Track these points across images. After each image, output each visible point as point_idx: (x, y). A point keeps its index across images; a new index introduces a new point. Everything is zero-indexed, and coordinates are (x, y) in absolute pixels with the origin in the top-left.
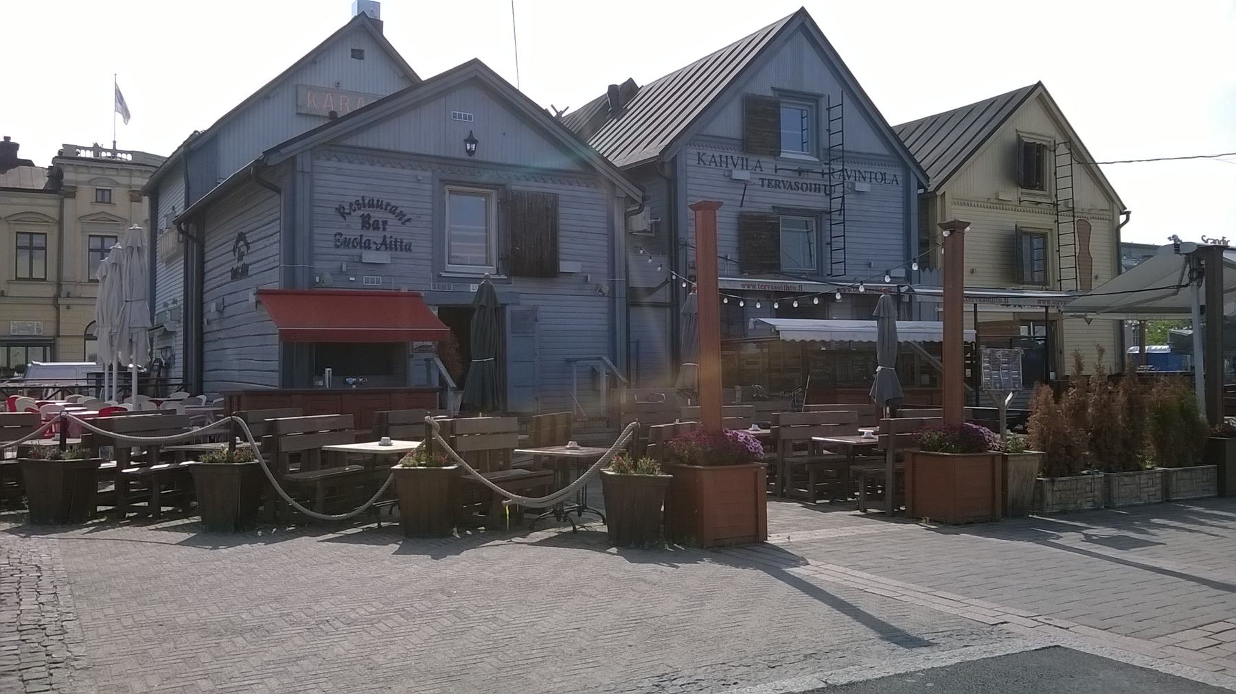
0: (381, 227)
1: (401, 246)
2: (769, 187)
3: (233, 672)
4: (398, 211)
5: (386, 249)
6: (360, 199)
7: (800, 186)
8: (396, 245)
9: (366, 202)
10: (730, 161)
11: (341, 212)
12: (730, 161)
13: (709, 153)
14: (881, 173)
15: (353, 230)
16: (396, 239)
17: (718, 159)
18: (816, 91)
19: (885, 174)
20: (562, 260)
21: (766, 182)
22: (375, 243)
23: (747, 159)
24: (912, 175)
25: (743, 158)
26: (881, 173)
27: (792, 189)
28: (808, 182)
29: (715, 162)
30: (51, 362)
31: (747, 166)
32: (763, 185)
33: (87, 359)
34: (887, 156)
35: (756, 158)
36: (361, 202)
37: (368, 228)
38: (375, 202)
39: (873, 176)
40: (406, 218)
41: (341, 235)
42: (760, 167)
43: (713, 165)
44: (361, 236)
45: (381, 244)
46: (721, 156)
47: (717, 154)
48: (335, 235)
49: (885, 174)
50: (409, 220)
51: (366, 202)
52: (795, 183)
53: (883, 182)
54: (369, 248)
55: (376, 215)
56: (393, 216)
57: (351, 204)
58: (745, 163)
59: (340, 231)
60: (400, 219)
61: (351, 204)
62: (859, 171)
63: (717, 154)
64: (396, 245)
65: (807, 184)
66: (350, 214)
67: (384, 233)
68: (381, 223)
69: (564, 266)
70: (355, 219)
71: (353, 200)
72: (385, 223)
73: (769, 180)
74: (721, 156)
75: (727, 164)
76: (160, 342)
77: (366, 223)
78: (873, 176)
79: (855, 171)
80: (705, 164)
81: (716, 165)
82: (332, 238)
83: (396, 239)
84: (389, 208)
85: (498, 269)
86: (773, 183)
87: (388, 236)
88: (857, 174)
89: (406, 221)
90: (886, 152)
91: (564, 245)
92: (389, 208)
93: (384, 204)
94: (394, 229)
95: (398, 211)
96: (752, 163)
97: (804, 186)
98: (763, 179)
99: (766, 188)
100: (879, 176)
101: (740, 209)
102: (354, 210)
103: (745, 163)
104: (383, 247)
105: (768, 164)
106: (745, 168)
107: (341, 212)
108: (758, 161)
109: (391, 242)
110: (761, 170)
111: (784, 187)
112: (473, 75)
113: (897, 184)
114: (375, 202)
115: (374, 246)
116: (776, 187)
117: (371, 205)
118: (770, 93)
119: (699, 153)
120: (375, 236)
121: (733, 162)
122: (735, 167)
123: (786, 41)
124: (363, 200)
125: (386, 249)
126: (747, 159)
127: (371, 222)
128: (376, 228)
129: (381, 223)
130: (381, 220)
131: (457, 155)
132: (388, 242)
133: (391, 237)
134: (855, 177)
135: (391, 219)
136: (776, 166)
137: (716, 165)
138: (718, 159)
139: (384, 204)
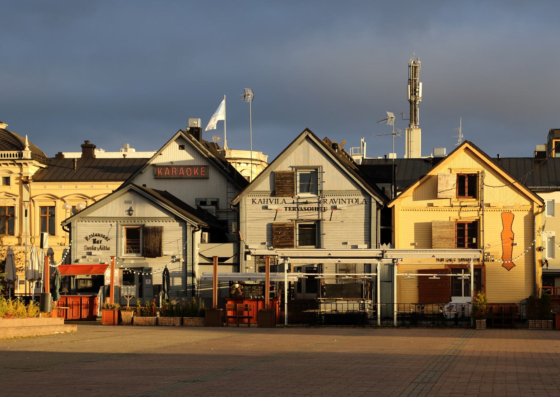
0: (99, 242)
1: (106, 248)
4: (105, 237)
5: (101, 250)
7: (307, 209)
8: (104, 248)
9: (95, 235)
10: (269, 201)
11: (86, 238)
12: (269, 201)
13: (258, 198)
14: (356, 199)
15: (90, 244)
16: (104, 246)
17: (263, 201)
19: (358, 199)
20: (165, 250)
21: (288, 209)
22: (97, 248)
23: (278, 199)
24: (373, 200)
26: (356, 199)
28: (311, 207)
29: (261, 202)
30: (339, 273)
31: (278, 202)
32: (286, 210)
33: (292, 270)
34: (356, 191)
35: (283, 198)
36: (93, 235)
37: (95, 243)
38: (98, 235)
39: (351, 201)
40: (108, 239)
41: (86, 246)
42: (285, 202)
43: (260, 203)
44: (93, 246)
46: (264, 199)
47: (262, 198)
48: (84, 246)
49: (358, 199)
50: (109, 240)
51: (95, 235)
53: (357, 203)
54: (95, 250)
55: (98, 238)
56: (104, 239)
57: (90, 236)
58: (277, 201)
59: (86, 245)
60: (106, 240)
61: (90, 236)
62: (342, 199)
64: (104, 248)
65: (311, 208)
66: (89, 239)
67: (101, 244)
68: (99, 241)
69: (165, 252)
70: (91, 241)
72: (101, 241)
73: (289, 208)
74: (264, 199)
76: (281, 261)
77: (95, 241)
78: (351, 201)
79: (339, 199)
80: (256, 203)
81: (262, 203)
82: (83, 247)
83: (104, 246)
84: (102, 236)
85: (142, 255)
87: (102, 245)
88: (341, 201)
89: (108, 240)
90: (355, 189)
92: (102, 236)
93: (101, 235)
94: (104, 243)
95: (105, 237)
96: (281, 199)
97: (309, 208)
100: (354, 201)
103: (277, 201)
104: (100, 249)
105: (289, 200)
106: (277, 203)
107: (87, 238)
108: (284, 200)
109: (103, 247)
112: (130, 188)
114: (98, 235)
115: (97, 249)
117: (96, 235)
119: (253, 199)
120: (97, 245)
121: (271, 201)
122: (271, 203)
123: (300, 144)
124: (94, 234)
125: (101, 250)
127: (96, 241)
128: (98, 243)
130: (99, 240)
131: (125, 216)
132: (102, 248)
133: (103, 246)
135: (104, 241)
137: (262, 203)
138: (263, 201)
139: (101, 235)
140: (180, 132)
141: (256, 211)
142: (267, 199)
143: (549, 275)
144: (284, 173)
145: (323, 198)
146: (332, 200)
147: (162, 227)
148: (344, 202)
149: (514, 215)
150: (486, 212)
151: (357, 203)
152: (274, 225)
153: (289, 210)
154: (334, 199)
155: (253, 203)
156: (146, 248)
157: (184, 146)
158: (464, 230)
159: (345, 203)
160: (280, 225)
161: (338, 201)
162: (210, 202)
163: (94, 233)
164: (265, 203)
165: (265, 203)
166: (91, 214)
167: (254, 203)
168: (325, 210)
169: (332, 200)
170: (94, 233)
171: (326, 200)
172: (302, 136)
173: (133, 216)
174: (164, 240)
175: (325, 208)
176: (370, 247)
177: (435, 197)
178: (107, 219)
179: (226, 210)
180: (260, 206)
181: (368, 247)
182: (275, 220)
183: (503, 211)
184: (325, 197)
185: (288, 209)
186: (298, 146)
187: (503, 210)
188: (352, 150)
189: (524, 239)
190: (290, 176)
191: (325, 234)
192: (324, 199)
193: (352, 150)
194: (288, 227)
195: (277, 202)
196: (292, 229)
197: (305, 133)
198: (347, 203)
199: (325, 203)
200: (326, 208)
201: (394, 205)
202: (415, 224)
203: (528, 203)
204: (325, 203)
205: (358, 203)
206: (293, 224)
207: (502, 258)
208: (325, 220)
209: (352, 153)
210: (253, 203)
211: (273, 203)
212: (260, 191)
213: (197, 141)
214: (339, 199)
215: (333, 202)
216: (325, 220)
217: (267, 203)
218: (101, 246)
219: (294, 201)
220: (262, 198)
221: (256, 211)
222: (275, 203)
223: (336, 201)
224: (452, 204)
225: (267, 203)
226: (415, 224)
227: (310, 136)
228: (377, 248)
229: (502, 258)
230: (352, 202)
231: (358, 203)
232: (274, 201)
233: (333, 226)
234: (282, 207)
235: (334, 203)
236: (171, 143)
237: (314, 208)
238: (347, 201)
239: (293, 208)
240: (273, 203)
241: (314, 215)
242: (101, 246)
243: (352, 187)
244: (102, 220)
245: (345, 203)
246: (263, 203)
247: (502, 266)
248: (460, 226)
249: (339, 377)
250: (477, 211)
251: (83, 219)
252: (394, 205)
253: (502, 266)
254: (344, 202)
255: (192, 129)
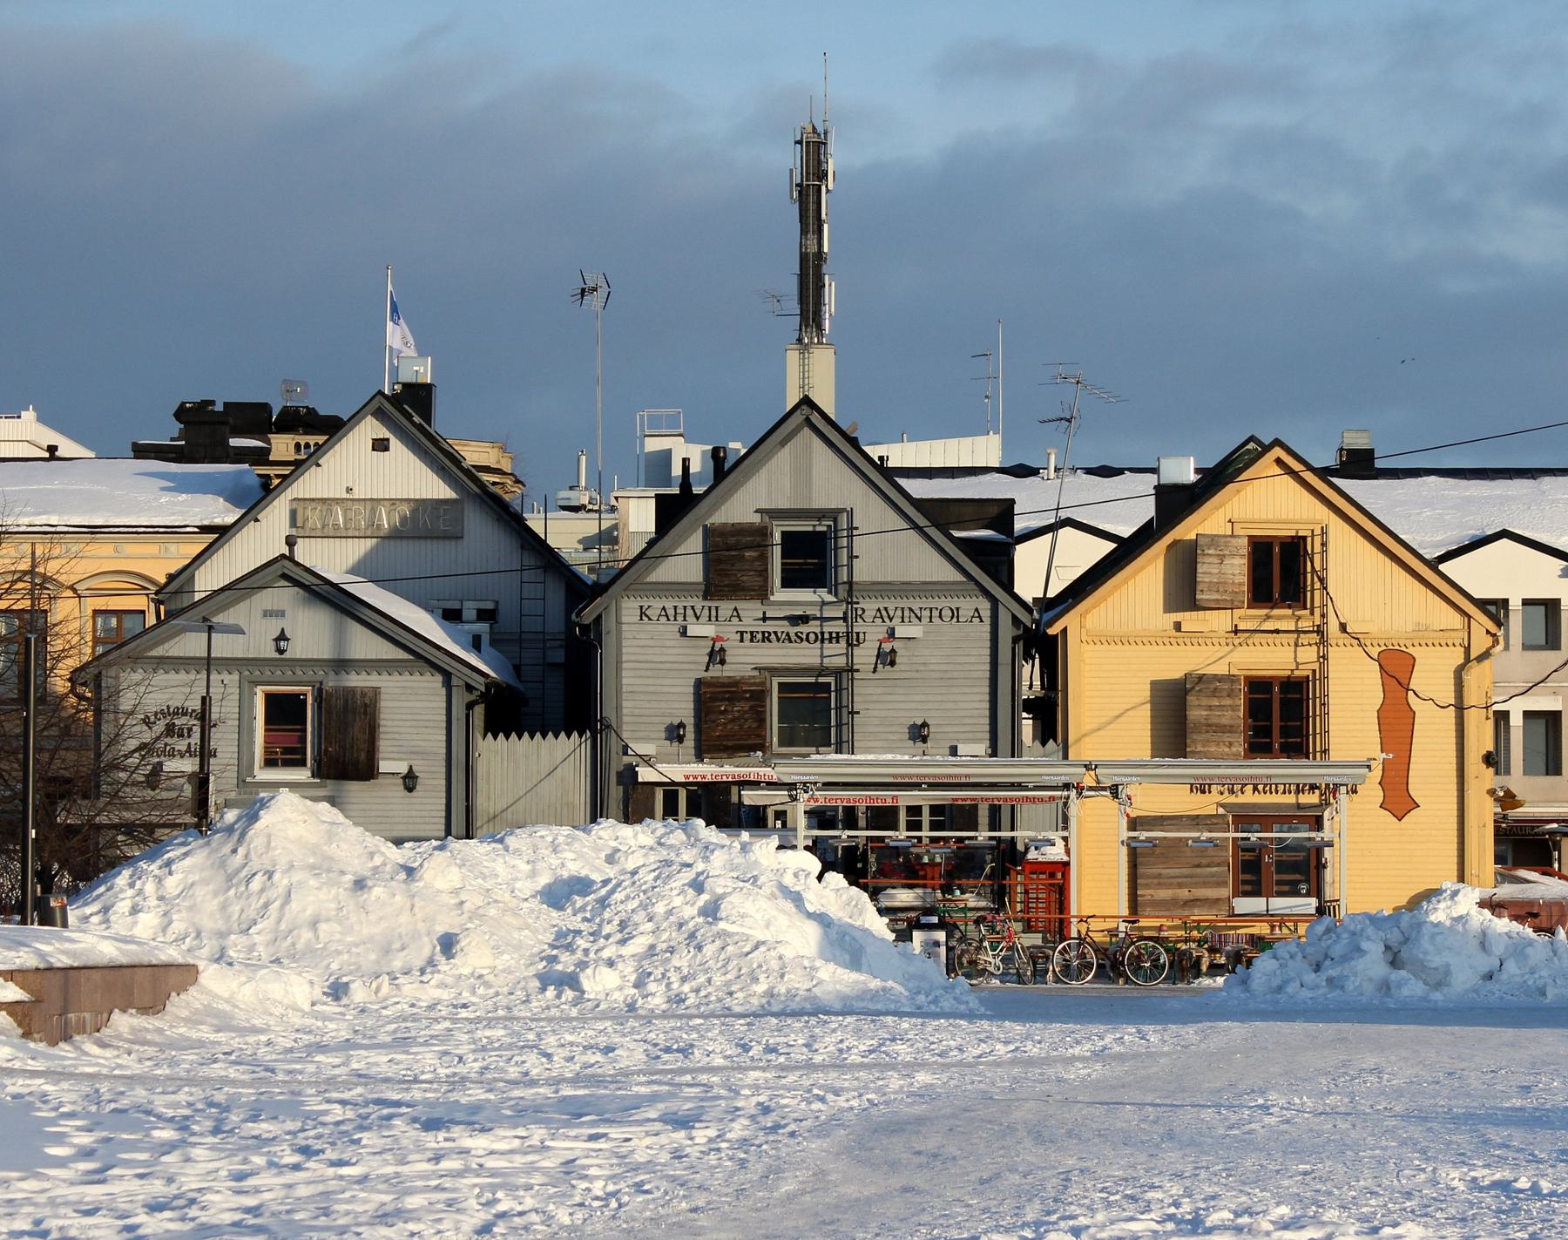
2: (752, 641)
3: (449, 1091)
6: (165, 708)
9: (171, 710)
10: (689, 612)
12: (689, 612)
13: (656, 605)
17: (671, 612)
18: (833, 505)
21: (747, 637)
23: (717, 608)
25: (710, 607)
27: (791, 642)
29: (667, 616)
31: (717, 617)
32: (742, 641)
39: (936, 613)
42: (738, 616)
43: (663, 619)
45: (186, 752)
49: (958, 609)
51: (171, 710)
52: (796, 634)
53: (955, 619)
61: (156, 714)
62: (911, 609)
63: (680, 605)
68: (185, 731)
69: (384, 766)
71: (158, 709)
73: (752, 633)
74: (675, 607)
75: (685, 617)
78: (936, 613)
79: (903, 609)
80: (650, 619)
81: (668, 620)
86: (759, 636)
88: (907, 613)
91: (384, 745)
92: (194, 715)
96: (726, 608)
98: (742, 633)
99: (747, 643)
100: (947, 613)
101: (704, 674)
102: (160, 719)
105: (751, 611)
106: (713, 619)
108: (736, 609)
110: (740, 620)
111: (778, 640)
113: (982, 621)
116: (763, 641)
118: (756, 519)
125: (191, 756)
126: (717, 608)
128: (181, 736)
129: (185, 731)
131: (267, 656)
134: (903, 617)
136: (764, 613)
137: (668, 620)
138: (671, 612)
140: (379, 396)
141: (651, 643)
142: (685, 607)
143: (1521, 830)
144: (739, 530)
145: (855, 606)
146: (879, 610)
147: (376, 691)
148: (917, 616)
149: (1414, 658)
150: (1335, 648)
151: (955, 619)
152: (705, 683)
153: (752, 641)
154: (886, 609)
155: (641, 619)
156: (326, 751)
157: (388, 440)
158: (1269, 702)
159: (920, 620)
160: (723, 685)
161: (899, 613)
162: (475, 612)
163: (168, 707)
164: (680, 618)
165: (680, 618)
166: (166, 646)
167: (644, 618)
168: (858, 640)
169: (879, 610)
170: (168, 707)
171: (863, 610)
172: (789, 421)
173: (287, 655)
174: (381, 729)
175: (858, 634)
176: (994, 754)
177: (1193, 605)
178: (380, 667)
179: (516, 637)
180: (674, 628)
181: (990, 751)
182: (707, 670)
183: (1382, 644)
184: (858, 603)
185: (747, 637)
186: (780, 450)
187: (1382, 643)
188: (642, 417)
189: (1149, 740)
190: (758, 535)
191: (858, 713)
192: (856, 609)
193: (642, 417)
194: (746, 691)
195: (714, 618)
196: (760, 696)
197: (799, 411)
198: (925, 620)
199: (859, 619)
200: (861, 636)
201: (1066, 628)
202: (1153, 683)
203: (1456, 620)
204: (859, 619)
205: (958, 621)
206: (763, 684)
207: (1380, 783)
208: (858, 671)
209: (642, 429)
210: (641, 619)
211: (704, 618)
212: (659, 583)
213: (426, 426)
214: (903, 609)
215: (882, 617)
216: (858, 671)
217: (685, 620)
218: (189, 744)
219: (764, 613)
220: (669, 605)
221: (651, 643)
222: (710, 620)
223: (891, 615)
224: (1236, 626)
225: (685, 620)
226: (1153, 683)
227: (816, 418)
228: (1013, 756)
229: (1380, 783)
230: (940, 617)
231: (958, 621)
232: (706, 612)
233: (879, 690)
234: (730, 632)
235: (887, 620)
236: (349, 432)
237: (834, 635)
238: (927, 613)
239: (763, 633)
240: (704, 618)
241: (835, 655)
242: (189, 744)
243: (953, 575)
244: (172, 667)
245: (920, 620)
246: (672, 619)
247: (1381, 807)
248: (1259, 687)
249: (699, 1188)
250: (1316, 644)
251: (136, 660)
252: (1066, 628)
253: (1381, 807)
254: (917, 616)
255: (408, 387)
